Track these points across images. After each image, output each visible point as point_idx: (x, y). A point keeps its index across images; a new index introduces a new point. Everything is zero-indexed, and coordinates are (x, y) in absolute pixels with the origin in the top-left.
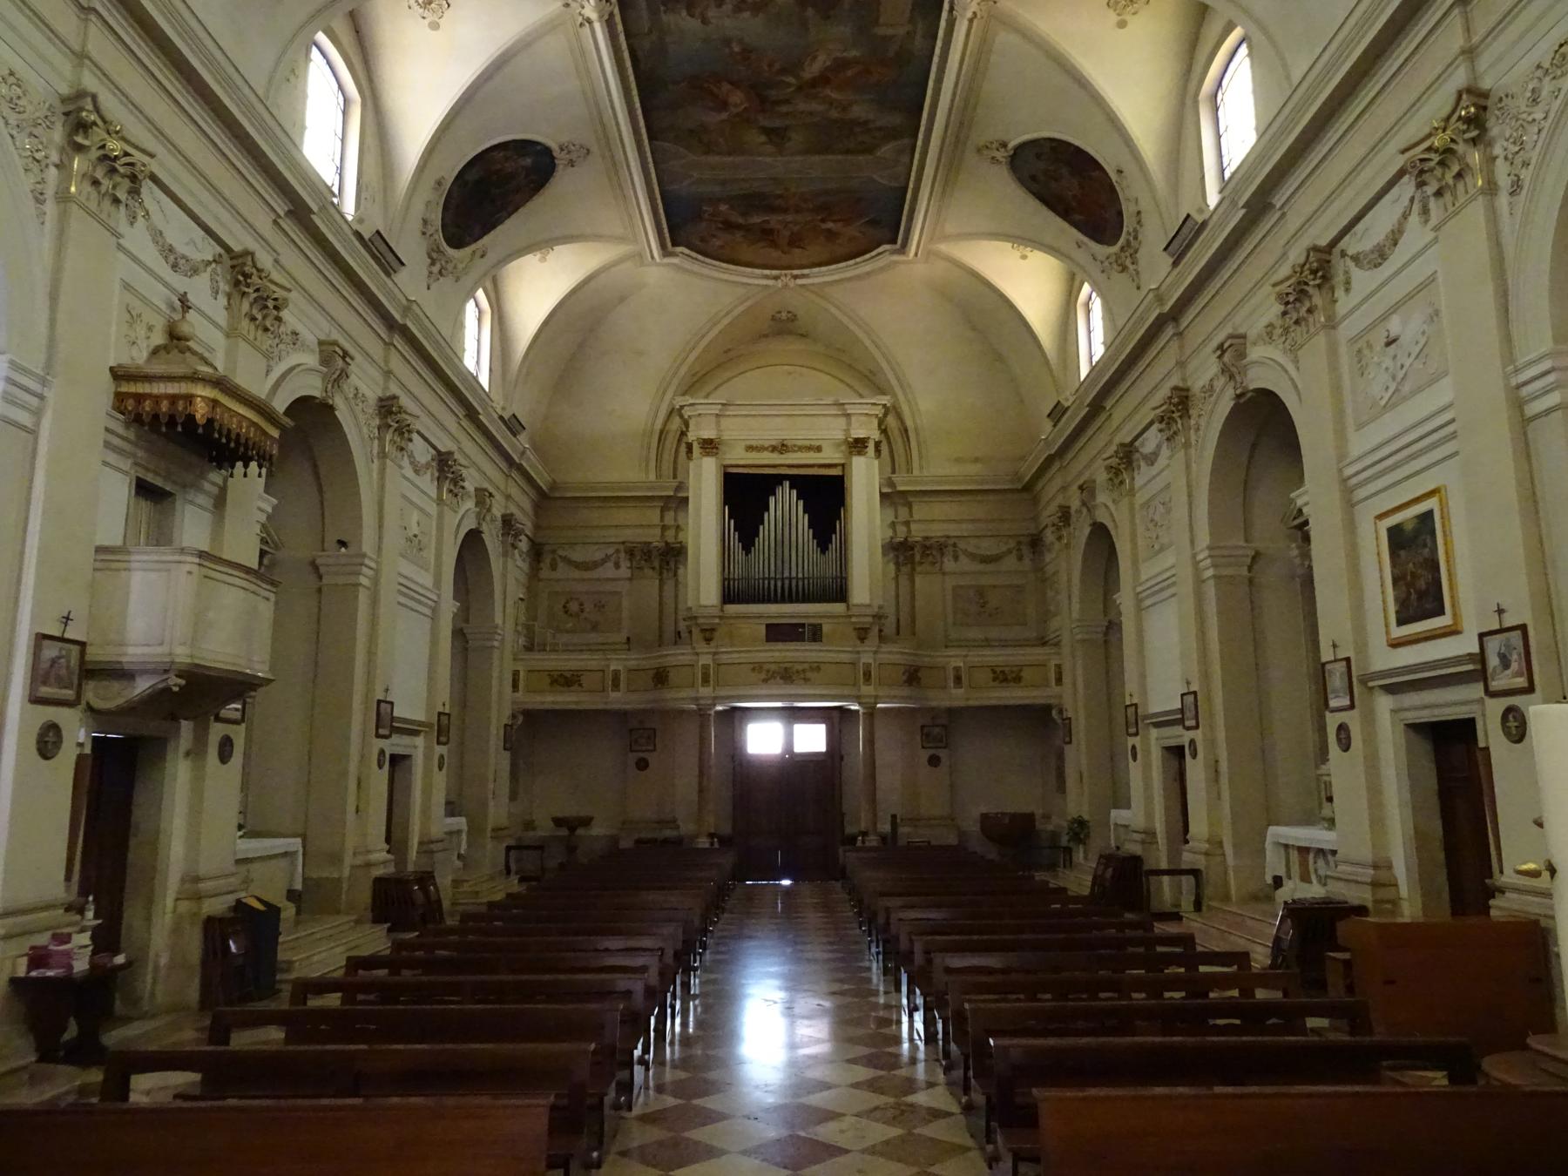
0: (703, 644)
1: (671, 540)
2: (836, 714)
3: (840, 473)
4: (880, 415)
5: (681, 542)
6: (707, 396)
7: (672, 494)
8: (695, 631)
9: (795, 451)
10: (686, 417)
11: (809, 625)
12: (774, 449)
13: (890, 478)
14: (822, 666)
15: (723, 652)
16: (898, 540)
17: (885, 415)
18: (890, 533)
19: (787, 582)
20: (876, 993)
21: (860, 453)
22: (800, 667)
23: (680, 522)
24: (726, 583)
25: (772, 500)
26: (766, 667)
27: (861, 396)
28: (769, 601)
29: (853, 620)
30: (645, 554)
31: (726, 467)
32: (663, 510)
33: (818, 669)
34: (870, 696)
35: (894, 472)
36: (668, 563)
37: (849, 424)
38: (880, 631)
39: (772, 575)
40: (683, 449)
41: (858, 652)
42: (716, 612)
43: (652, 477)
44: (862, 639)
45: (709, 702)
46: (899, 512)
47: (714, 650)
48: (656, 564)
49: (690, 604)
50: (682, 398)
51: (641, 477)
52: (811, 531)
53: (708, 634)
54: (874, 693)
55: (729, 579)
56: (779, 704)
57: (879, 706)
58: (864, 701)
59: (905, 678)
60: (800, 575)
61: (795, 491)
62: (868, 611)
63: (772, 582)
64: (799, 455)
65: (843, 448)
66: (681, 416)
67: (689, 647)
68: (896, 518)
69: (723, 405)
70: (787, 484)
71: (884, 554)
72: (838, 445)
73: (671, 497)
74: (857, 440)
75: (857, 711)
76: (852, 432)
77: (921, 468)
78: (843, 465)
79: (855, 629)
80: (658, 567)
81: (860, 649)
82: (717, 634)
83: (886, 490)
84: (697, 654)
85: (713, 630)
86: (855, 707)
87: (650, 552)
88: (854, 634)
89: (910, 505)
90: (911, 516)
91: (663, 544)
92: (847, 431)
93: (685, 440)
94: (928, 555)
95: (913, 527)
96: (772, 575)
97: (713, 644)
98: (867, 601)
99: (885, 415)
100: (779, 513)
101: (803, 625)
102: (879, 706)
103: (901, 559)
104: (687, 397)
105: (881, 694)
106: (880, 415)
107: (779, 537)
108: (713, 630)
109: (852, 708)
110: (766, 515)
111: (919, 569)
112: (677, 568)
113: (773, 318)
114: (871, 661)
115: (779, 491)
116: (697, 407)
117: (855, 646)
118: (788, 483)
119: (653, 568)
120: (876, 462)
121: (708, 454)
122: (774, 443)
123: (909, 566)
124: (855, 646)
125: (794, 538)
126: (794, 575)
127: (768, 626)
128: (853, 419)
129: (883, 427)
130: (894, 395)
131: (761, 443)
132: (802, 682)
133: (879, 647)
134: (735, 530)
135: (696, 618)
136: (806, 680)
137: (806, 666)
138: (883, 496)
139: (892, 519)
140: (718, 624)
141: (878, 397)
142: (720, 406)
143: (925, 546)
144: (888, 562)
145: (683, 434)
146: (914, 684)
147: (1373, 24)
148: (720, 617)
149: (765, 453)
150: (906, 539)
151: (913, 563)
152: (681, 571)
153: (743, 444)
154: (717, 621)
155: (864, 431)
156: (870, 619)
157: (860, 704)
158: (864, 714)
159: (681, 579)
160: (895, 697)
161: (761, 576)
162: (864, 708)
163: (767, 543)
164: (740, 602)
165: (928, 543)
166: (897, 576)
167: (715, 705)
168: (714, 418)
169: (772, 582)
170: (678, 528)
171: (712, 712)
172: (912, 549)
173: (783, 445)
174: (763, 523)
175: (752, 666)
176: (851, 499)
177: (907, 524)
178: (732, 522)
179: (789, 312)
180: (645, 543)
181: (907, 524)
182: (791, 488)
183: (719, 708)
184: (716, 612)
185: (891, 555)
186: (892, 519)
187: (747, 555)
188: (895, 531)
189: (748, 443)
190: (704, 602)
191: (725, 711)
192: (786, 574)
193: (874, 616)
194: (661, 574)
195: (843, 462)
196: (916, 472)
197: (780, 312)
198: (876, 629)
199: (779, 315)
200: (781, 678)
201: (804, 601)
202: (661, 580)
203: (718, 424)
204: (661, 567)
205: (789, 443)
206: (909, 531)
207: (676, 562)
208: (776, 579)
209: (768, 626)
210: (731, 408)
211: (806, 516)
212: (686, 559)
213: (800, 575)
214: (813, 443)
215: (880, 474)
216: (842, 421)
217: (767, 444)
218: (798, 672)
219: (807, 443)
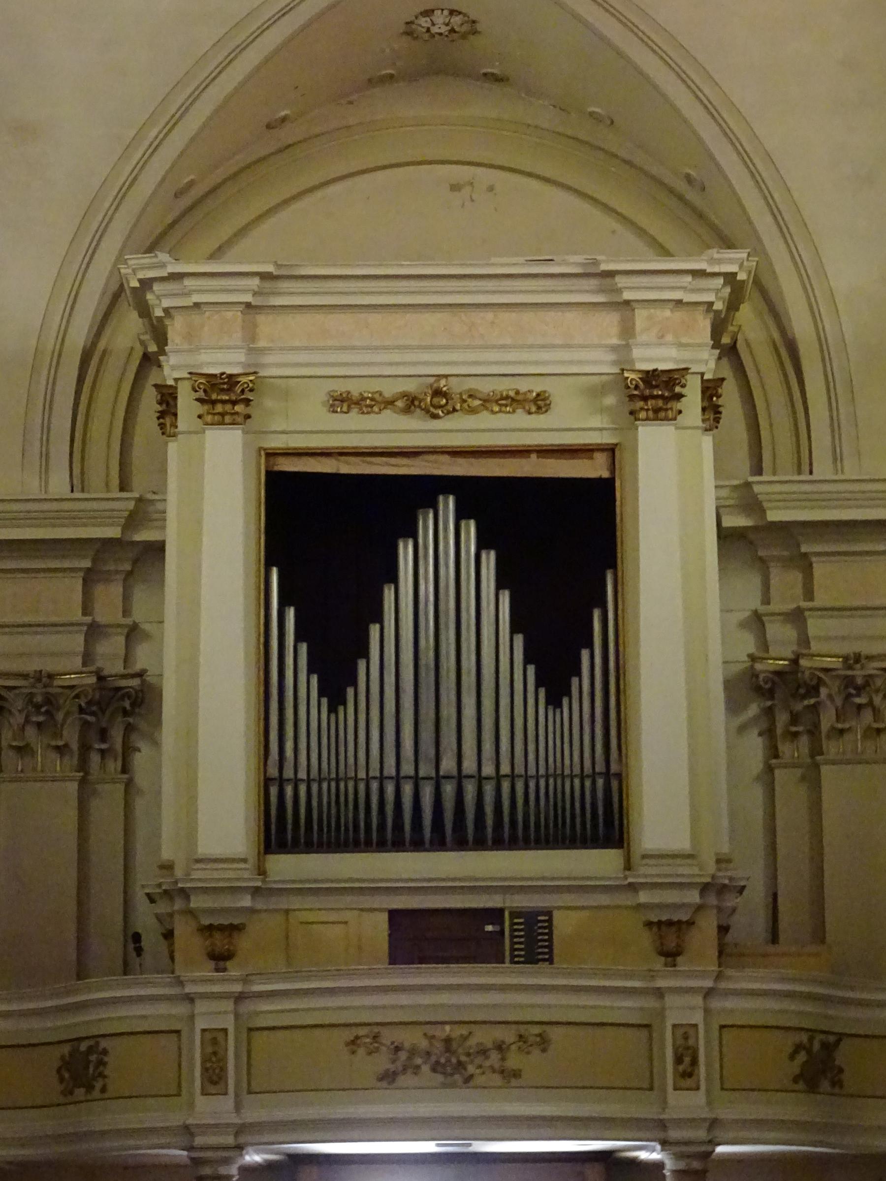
0: (207, 970)
1: (113, 667)
2: (594, 1176)
3: (606, 474)
4: (719, 306)
5: (140, 674)
6: (216, 254)
7: (114, 532)
8: (183, 929)
9: (473, 411)
10: (158, 313)
11: (515, 914)
12: (411, 403)
13: (748, 485)
14: (556, 1034)
15: (260, 995)
16: (773, 665)
17: (733, 305)
18: (747, 644)
19: (449, 789)
20: (218, 395)
21: (658, 415)
22: (483, 1037)
23: (138, 614)
24: (274, 791)
25: (405, 552)
26: (389, 1036)
27: (665, 252)
28: (398, 845)
29: (644, 897)
30: (38, 707)
31: (271, 455)
32: (90, 578)
33: (543, 1043)
34: (691, 1122)
35: (758, 470)
36: (103, 735)
37: (627, 331)
38: (723, 930)
39: (408, 769)
40: (149, 403)
41: (660, 993)
42: (246, 876)
43: (59, 483)
44: (671, 955)
45: (230, 1140)
46: (774, 581)
47: (237, 988)
48: (71, 736)
49: (166, 854)
50: (147, 260)
51: (33, 488)
52: (519, 640)
53: (220, 942)
54: (706, 1114)
55: (281, 782)
56: (429, 1147)
57: (720, 1149)
58: (674, 1134)
59: (795, 1067)
60: (488, 770)
61: (472, 524)
62: (686, 871)
63: (408, 789)
64: (485, 420)
65: (610, 400)
66: (144, 311)
67: (167, 978)
68: (766, 601)
69: (265, 276)
70: (448, 505)
71: (733, 706)
72: (595, 392)
73: (111, 540)
74: (650, 377)
75: (658, 1166)
76: (636, 353)
77: (837, 458)
78: (611, 450)
79: (649, 924)
80: (75, 746)
81: (661, 983)
82: (244, 943)
83: (736, 521)
84: (190, 999)
85: (234, 929)
86: (650, 1154)
87: (49, 700)
88: (646, 939)
89: (805, 564)
90: (809, 594)
91: (93, 680)
92: (623, 350)
93: (153, 378)
94: (860, 707)
95: (815, 626)
96: (408, 769)
97: (234, 971)
98: (682, 843)
99: (733, 305)
100: (427, 589)
101: (495, 915)
102: (720, 1149)
103: (782, 719)
104: (163, 257)
105: (725, 1113)
106: (719, 306)
107: (428, 657)
108: (234, 929)
109: (643, 1155)
110: (389, 594)
111: (832, 748)
112: (128, 750)
113: (409, 31)
114: (697, 1018)
115: (426, 524)
116: (187, 282)
117: (652, 975)
118: (451, 500)
119: (61, 750)
120: (707, 442)
121: (221, 421)
122: (411, 386)
123: (804, 740)
124: (652, 975)
125: (448, 711)
126: (469, 765)
127: (394, 915)
128: (641, 316)
129: (726, 340)
130: (758, 249)
131: (374, 386)
132: (497, 1079)
133: (719, 977)
134: (298, 638)
135: (185, 893)
136: (510, 1075)
137: (508, 1035)
138: (725, 536)
139: (754, 602)
140: (252, 911)
141: (714, 253)
142: (255, 282)
143: (849, 681)
144: (742, 729)
145: (149, 361)
146: (825, 1085)
147: (813, 493)
148: (256, 892)
149: (387, 413)
150: (795, 662)
151: (814, 732)
152: (141, 760)
153: (320, 392)
154: (246, 902)
155: (673, 352)
156: (693, 897)
157: (665, 1144)
158: (675, 1172)
159: (141, 778)
160: (759, 1123)
161: (375, 772)
162: (679, 1156)
163: (390, 679)
164: (310, 847)
165: (858, 674)
166: (769, 770)
167: (240, 1148)
168: (235, 316)
169: (408, 789)
170: (133, 633)
171: (233, 1170)
172: (814, 690)
173: (438, 393)
174: (378, 618)
175: (348, 1035)
176: (790, 320)
177: (797, 617)
178: (291, 613)
179: (452, 12)
180: (39, 676)
181: (797, 617)
182: (460, 516)
183: (253, 1157)
184: (246, 876)
185: (753, 710)
186: (754, 602)
187: (332, 709)
188: (764, 644)
189: (341, 387)
190: (206, 846)
191: (269, 1166)
192: (448, 764)
193: (705, 888)
194: (83, 765)
195: (607, 439)
196: (823, 468)
197: (428, 13)
198: (708, 924)
199: (424, 22)
200: (436, 1068)
201: (499, 844)
202: (83, 782)
203: (251, 334)
204: (85, 748)
205: (456, 387)
206: (804, 640)
207: (129, 729)
208: (416, 780)
209: (394, 915)
210: (284, 285)
211: (505, 598)
212: (158, 723)
213: (488, 770)
214: (523, 386)
215: (719, 472)
216: (610, 322)
217: (390, 389)
218: (483, 1052)
219: (505, 386)
